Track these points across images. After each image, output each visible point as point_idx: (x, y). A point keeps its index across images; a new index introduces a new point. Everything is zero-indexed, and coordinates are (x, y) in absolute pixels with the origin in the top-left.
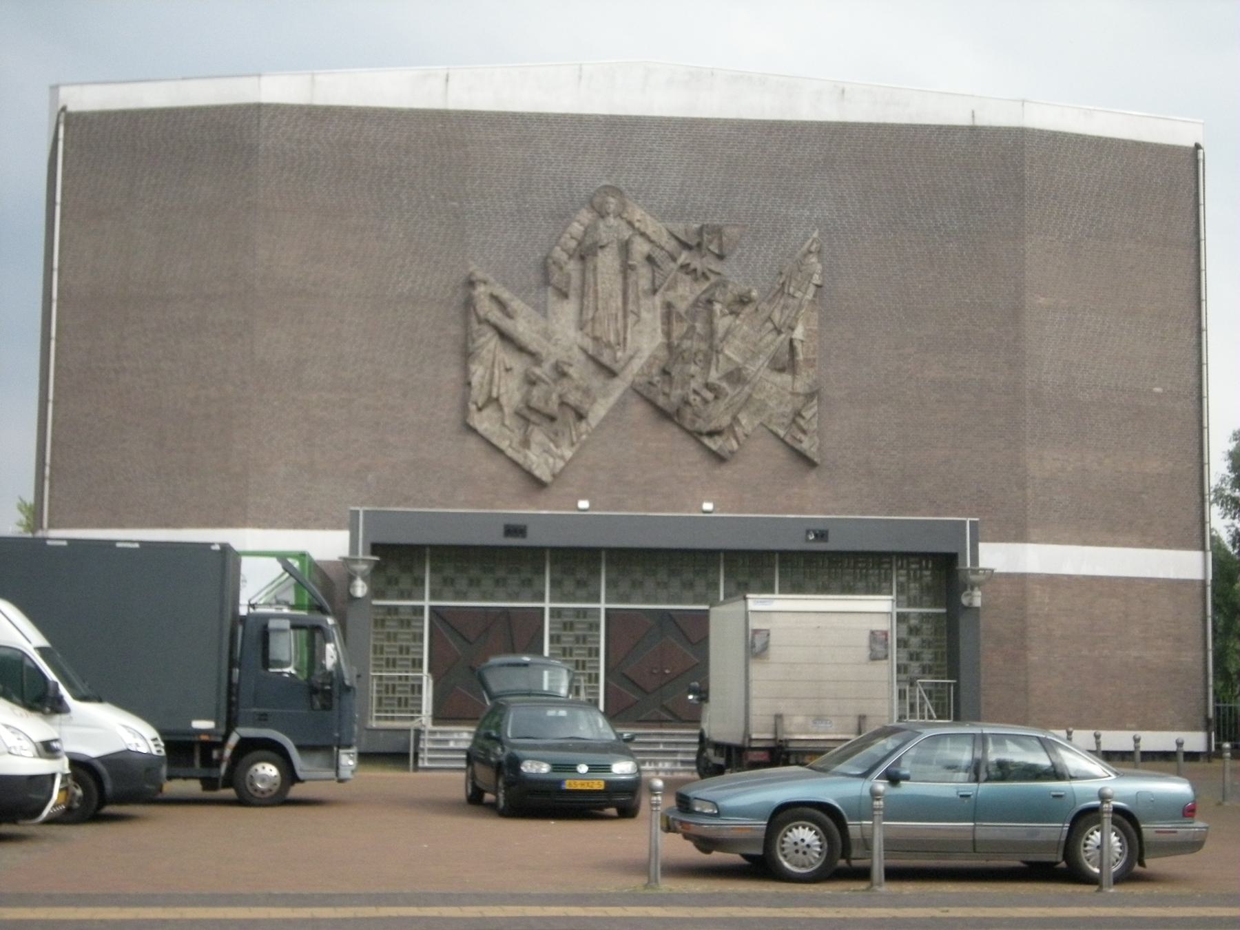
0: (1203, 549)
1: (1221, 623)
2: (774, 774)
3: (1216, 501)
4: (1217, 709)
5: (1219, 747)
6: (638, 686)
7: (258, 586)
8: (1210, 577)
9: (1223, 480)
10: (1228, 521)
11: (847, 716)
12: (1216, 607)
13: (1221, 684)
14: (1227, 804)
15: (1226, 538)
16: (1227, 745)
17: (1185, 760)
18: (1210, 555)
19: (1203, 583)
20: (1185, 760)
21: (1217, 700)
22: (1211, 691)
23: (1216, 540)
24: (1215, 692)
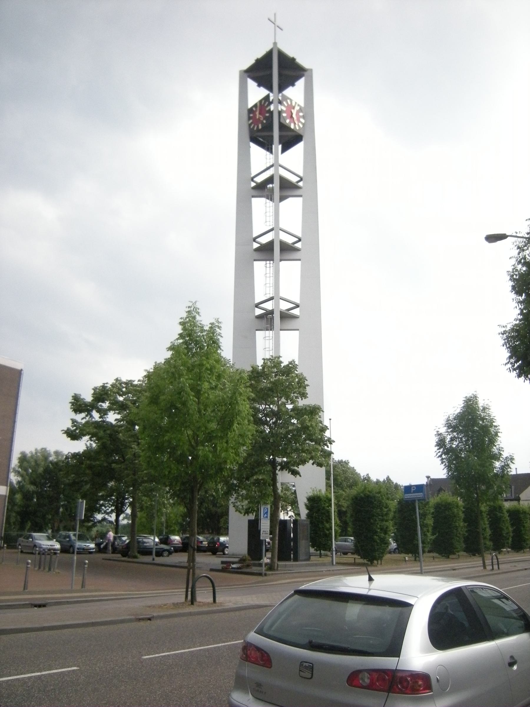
0: (7, 486)
1: (10, 507)
2: (444, 588)
3: (13, 472)
4: (5, 534)
5: (3, 545)
6: (26, 575)
7: (433, 537)
8: (8, 494)
9: (16, 466)
10: (16, 477)
11: (40, 559)
12: (8, 502)
13: (7, 526)
14: (3, 563)
15: (15, 482)
16: (5, 545)
17: (250, 522)
18: (9, 488)
19: (6, 496)
20: (250, 522)
21: (5, 531)
22: (4, 528)
23: (11, 483)
24: (5, 529)
